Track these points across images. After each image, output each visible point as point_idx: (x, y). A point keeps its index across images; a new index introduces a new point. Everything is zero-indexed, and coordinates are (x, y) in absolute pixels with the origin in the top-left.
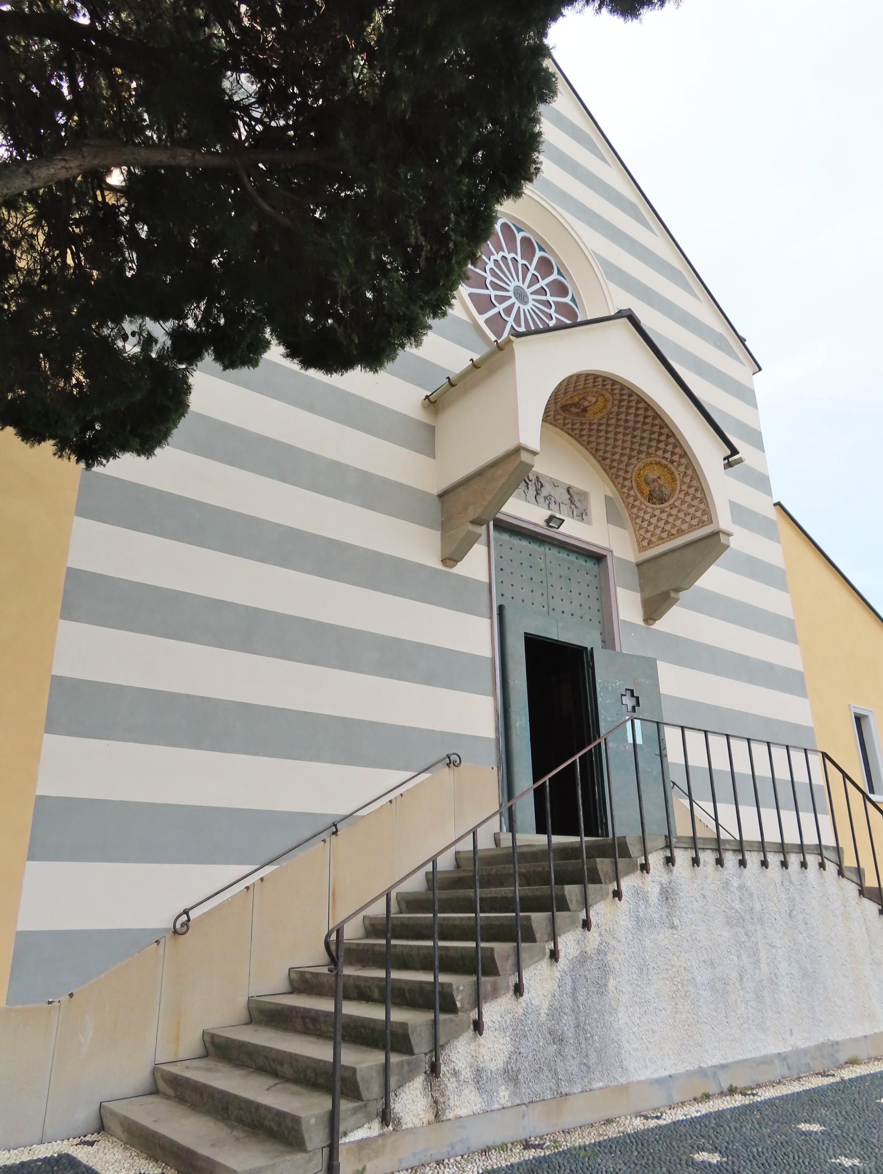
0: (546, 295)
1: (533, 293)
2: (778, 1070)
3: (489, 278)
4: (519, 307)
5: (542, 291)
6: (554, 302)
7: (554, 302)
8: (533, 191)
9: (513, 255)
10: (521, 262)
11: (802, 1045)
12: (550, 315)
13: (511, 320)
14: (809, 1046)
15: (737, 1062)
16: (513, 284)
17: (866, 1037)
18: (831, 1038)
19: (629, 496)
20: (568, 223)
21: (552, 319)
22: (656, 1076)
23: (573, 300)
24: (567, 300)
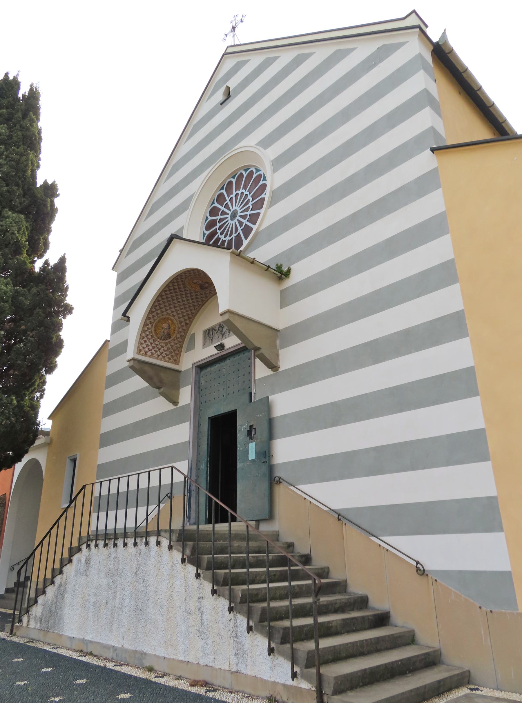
0: (227, 203)
1: (230, 210)
2: (109, 654)
3: (234, 235)
4: (240, 213)
5: (227, 206)
6: (228, 198)
7: (228, 198)
8: (224, 157)
9: (218, 230)
10: (218, 225)
11: (127, 647)
12: (235, 195)
13: (248, 213)
14: (129, 649)
15: (96, 642)
16: (237, 208)
17: (164, 658)
18: (143, 650)
19: (181, 336)
20: (203, 182)
21: (237, 193)
22: (70, 635)
23: (222, 189)
24: (224, 191)
